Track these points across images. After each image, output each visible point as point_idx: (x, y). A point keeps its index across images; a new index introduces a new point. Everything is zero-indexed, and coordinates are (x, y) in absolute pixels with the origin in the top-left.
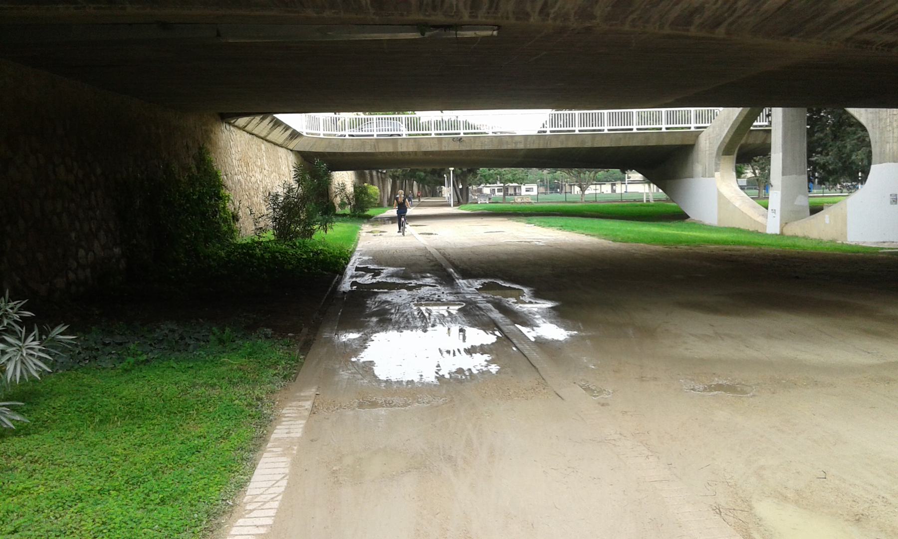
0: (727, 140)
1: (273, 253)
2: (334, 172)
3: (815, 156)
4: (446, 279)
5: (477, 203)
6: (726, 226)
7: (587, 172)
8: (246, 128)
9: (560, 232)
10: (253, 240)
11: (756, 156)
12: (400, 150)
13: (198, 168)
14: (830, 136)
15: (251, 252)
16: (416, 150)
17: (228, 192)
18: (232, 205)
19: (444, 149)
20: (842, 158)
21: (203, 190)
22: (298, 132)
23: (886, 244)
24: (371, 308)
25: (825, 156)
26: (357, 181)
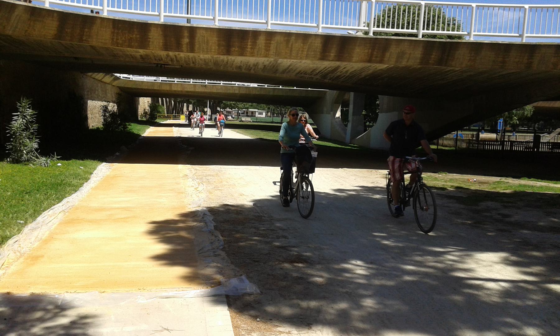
11: (302, 135)
19: (197, 90)
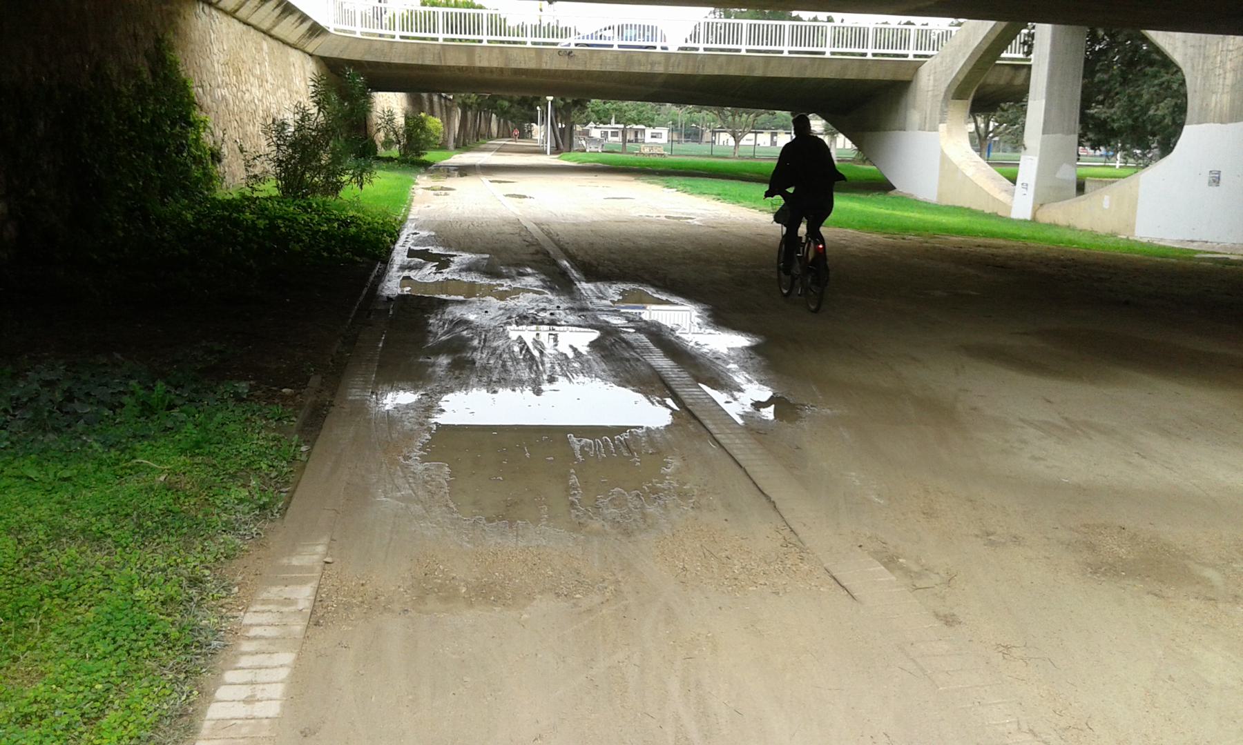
0: (961, 78)
1: (272, 219)
2: (375, 94)
3: (1095, 107)
4: (560, 282)
5: (585, 151)
6: (950, 204)
7: (744, 115)
8: (238, 14)
9: (718, 202)
10: (243, 195)
11: (1005, 102)
12: (478, 64)
13: (154, 73)
14: (1119, 79)
15: (235, 215)
16: (503, 66)
17: (205, 114)
18: (210, 137)
19: (544, 66)
20: (1133, 112)
21: (161, 108)
22: (321, 27)
23: (1195, 244)
24: (437, 334)
25: (1108, 108)
26: (410, 108)
